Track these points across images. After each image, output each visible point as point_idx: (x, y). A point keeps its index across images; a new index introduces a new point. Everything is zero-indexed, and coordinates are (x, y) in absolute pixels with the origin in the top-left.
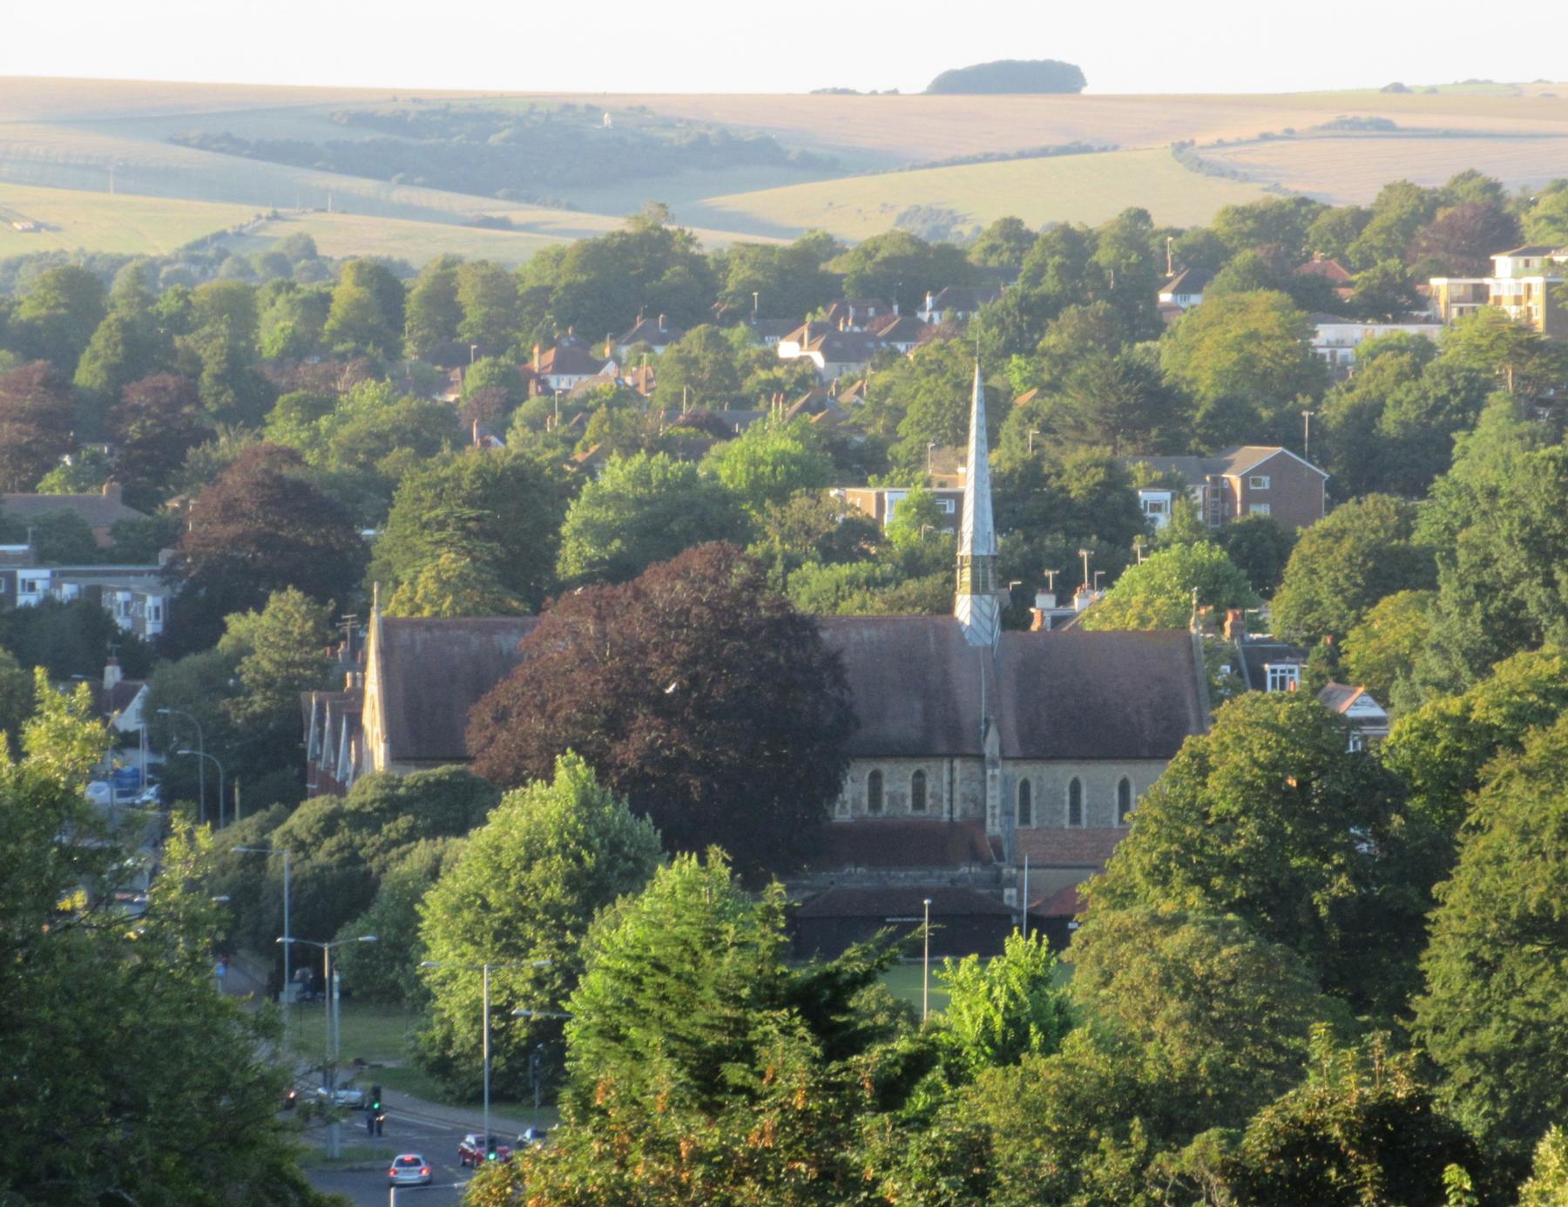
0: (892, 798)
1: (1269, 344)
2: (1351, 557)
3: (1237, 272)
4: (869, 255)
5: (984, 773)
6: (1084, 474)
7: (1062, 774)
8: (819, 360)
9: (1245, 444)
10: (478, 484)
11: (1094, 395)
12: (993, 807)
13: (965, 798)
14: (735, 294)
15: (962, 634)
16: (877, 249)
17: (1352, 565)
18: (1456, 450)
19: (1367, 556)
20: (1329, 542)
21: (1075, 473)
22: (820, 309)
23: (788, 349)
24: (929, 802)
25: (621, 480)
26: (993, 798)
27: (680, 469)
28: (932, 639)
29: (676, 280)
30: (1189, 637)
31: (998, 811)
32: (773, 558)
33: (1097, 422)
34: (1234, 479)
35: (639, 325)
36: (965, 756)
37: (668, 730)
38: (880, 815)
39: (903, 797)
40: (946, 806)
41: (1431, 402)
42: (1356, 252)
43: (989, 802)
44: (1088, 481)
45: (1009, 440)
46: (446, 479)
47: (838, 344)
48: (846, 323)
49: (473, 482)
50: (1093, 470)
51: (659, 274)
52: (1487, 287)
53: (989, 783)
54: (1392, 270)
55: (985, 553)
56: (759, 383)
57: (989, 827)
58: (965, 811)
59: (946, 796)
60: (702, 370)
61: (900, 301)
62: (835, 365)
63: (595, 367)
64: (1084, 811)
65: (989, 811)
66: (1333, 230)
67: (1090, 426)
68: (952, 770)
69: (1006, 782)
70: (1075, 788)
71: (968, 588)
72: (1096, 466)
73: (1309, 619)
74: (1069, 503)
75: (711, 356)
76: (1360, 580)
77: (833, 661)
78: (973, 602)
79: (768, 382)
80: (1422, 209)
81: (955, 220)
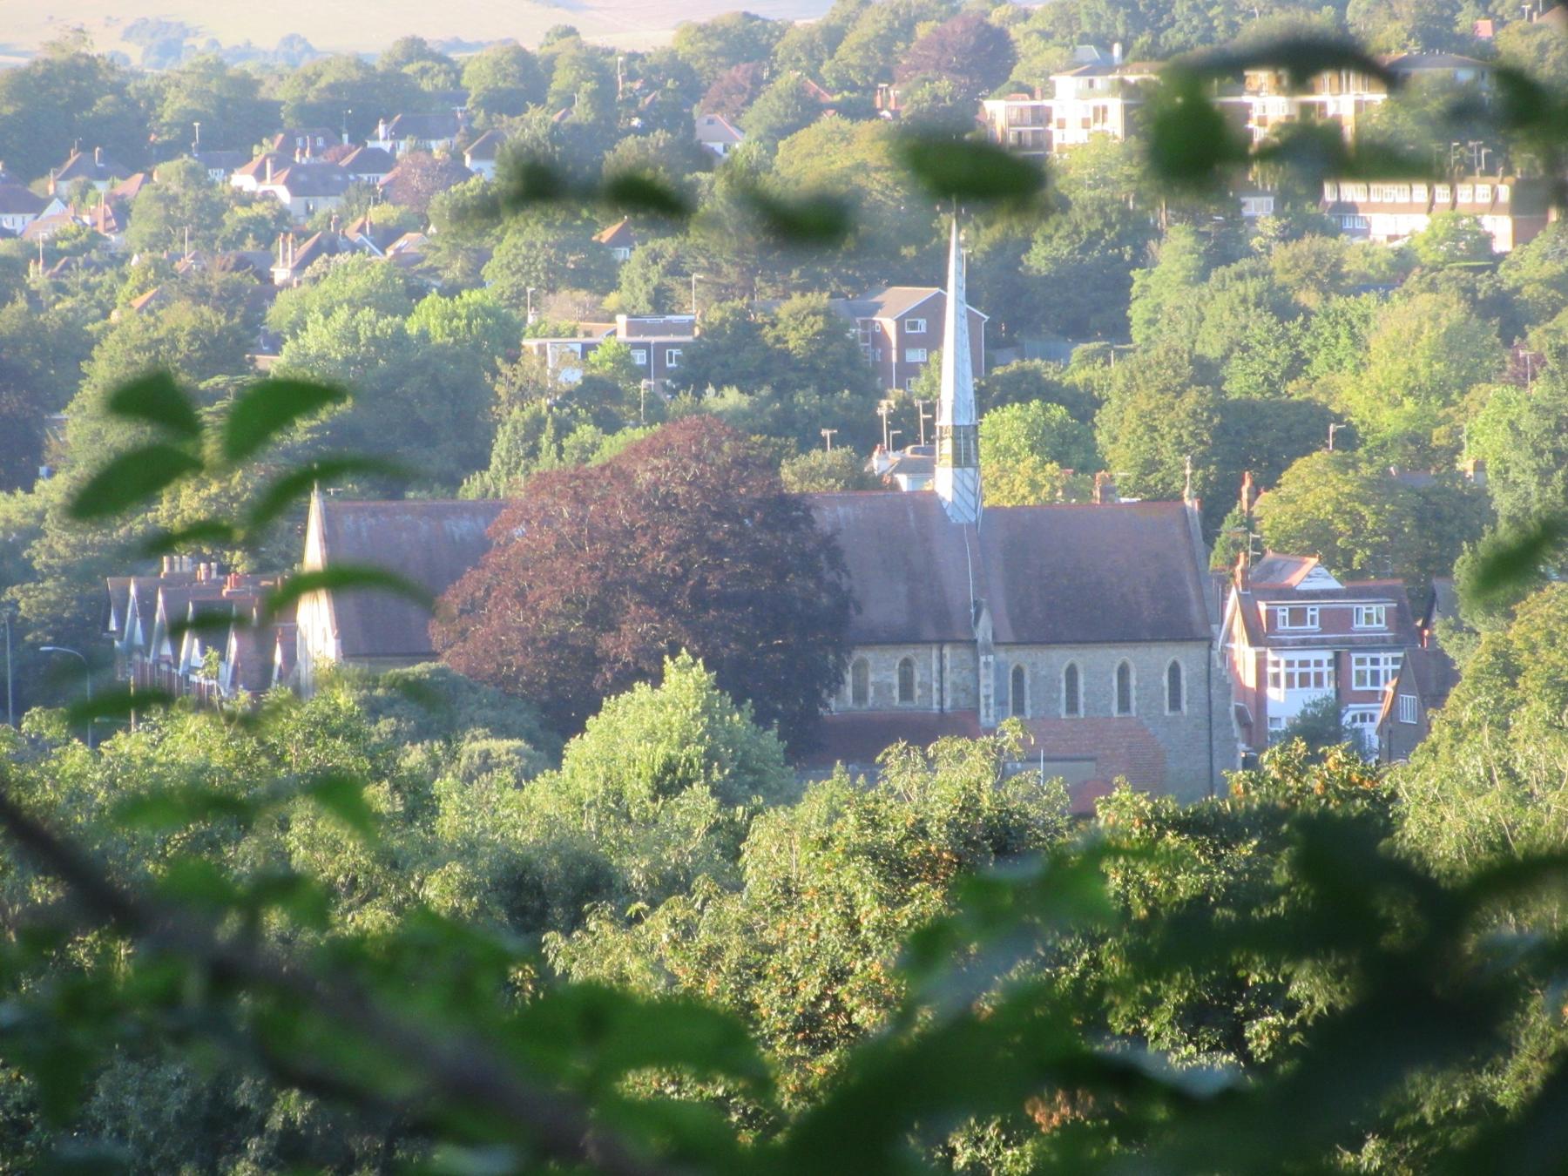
0: (878, 690)
1: (878, 176)
2: (1195, 412)
3: (779, 97)
4: (309, 82)
5: (977, 660)
6: (802, 324)
7: (1059, 658)
8: (284, 195)
9: (889, 285)
10: (197, 345)
11: (730, 235)
12: (987, 697)
13: (955, 686)
14: (171, 126)
15: (943, 510)
16: (319, 75)
17: (1197, 421)
18: (1135, 290)
19: (1212, 412)
20: (1169, 397)
21: (792, 323)
22: (265, 141)
23: (243, 180)
24: (918, 692)
25: (326, 338)
26: (987, 686)
27: (389, 325)
28: (912, 516)
29: (108, 110)
30: (1184, 510)
31: (992, 700)
32: (544, 421)
33: (734, 264)
34: (888, 325)
35: (73, 158)
36: (955, 642)
37: (662, 620)
38: (864, 707)
39: (890, 687)
40: (936, 696)
41: (1085, 236)
42: (830, 71)
43: (983, 691)
44: (806, 330)
45: (631, 283)
46: (161, 341)
47: (302, 178)
48: (303, 154)
49: (190, 344)
50: (811, 319)
51: (88, 103)
52: (1049, 109)
53: (982, 671)
54: (941, 93)
55: (966, 423)
56: (240, 221)
57: (983, 719)
58: (955, 700)
59: (935, 686)
60: (183, 208)
61: (349, 129)
62: (302, 200)
63: (36, 206)
64: (1082, 699)
65: (982, 700)
66: (802, 47)
67: (726, 268)
68: (941, 658)
69: (999, 671)
70: (1072, 673)
71: (950, 462)
72: (815, 314)
73: (1151, 480)
74: (786, 355)
75: (191, 194)
76: (1206, 437)
77: (830, 548)
78: (955, 475)
79: (249, 220)
80: (896, 24)
81: (186, 33)
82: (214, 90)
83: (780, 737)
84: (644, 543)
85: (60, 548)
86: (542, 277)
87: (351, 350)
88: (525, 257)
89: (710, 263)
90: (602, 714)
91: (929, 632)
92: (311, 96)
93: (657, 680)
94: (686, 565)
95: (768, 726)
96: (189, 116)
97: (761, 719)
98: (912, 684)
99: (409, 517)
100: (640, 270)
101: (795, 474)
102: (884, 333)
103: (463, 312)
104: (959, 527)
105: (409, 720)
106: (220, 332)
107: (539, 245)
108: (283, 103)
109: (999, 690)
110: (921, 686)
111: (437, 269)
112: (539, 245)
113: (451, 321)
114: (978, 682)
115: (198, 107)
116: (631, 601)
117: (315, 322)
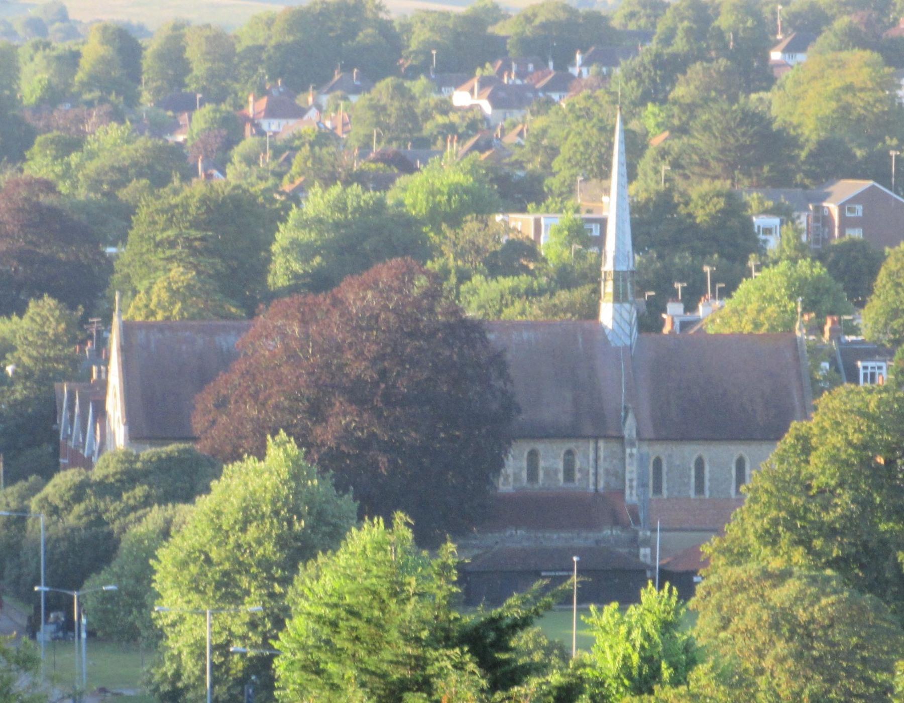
0: (547, 473)
3: (836, 35)
4: (528, 19)
5: (624, 452)
6: (708, 203)
7: (689, 452)
8: (487, 107)
10: (203, 210)
11: (716, 137)
12: (631, 480)
13: (607, 472)
14: (417, 53)
15: (605, 337)
21: (700, 202)
22: (488, 65)
23: (461, 98)
24: (578, 475)
25: (322, 207)
26: (631, 472)
28: (580, 340)
29: (368, 41)
30: (795, 339)
31: (635, 483)
32: (449, 272)
36: (606, 437)
38: (536, 486)
39: (556, 472)
40: (592, 479)
43: (628, 476)
44: (711, 209)
45: (645, 174)
47: (502, 94)
48: (509, 76)
49: (198, 208)
50: (715, 200)
53: (628, 460)
58: (607, 483)
59: (592, 471)
61: (554, 58)
62: (500, 112)
64: (707, 484)
65: (627, 483)
68: (597, 449)
69: (642, 460)
71: (611, 298)
74: (694, 226)
75: (396, 104)
77: (498, 360)
78: (615, 310)
82: (451, 26)
83: (355, 499)
84: (349, 356)
85: (25, 360)
86: (595, 168)
87: (342, 217)
88: (582, 153)
89: (701, 159)
90: (223, 478)
91: (588, 429)
92: (529, 31)
93: (261, 454)
94: (383, 374)
95: (346, 491)
96: (428, 45)
97: (340, 486)
98: (565, 472)
99: (187, 334)
100: (652, 164)
101: (540, 309)
102: (830, 215)
103: (446, 190)
104: (617, 349)
105: (158, 487)
106: (223, 198)
107: (593, 144)
108: (507, 37)
109: (642, 477)
110: (580, 470)
111: (522, 162)
112: (593, 144)
113: (434, 196)
114: (624, 468)
115: (438, 39)
116: (338, 402)
117: (315, 194)
